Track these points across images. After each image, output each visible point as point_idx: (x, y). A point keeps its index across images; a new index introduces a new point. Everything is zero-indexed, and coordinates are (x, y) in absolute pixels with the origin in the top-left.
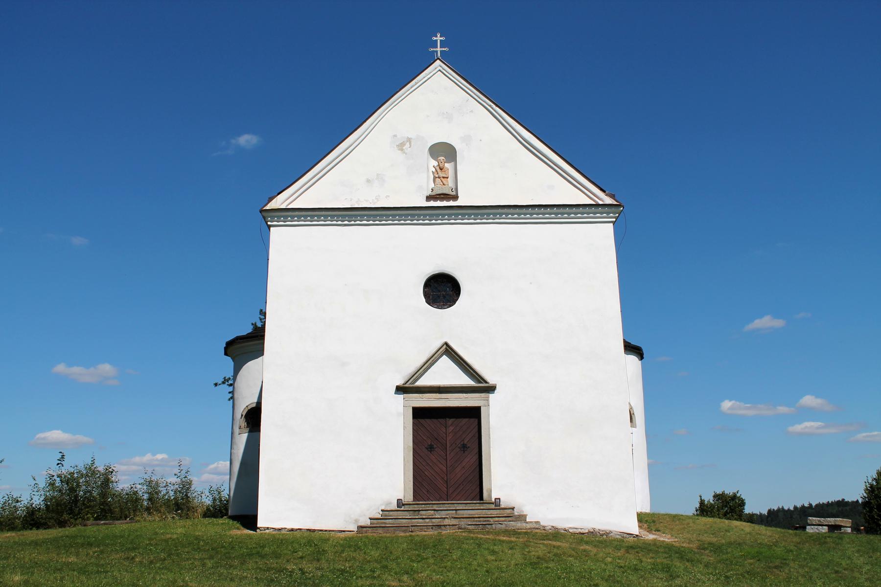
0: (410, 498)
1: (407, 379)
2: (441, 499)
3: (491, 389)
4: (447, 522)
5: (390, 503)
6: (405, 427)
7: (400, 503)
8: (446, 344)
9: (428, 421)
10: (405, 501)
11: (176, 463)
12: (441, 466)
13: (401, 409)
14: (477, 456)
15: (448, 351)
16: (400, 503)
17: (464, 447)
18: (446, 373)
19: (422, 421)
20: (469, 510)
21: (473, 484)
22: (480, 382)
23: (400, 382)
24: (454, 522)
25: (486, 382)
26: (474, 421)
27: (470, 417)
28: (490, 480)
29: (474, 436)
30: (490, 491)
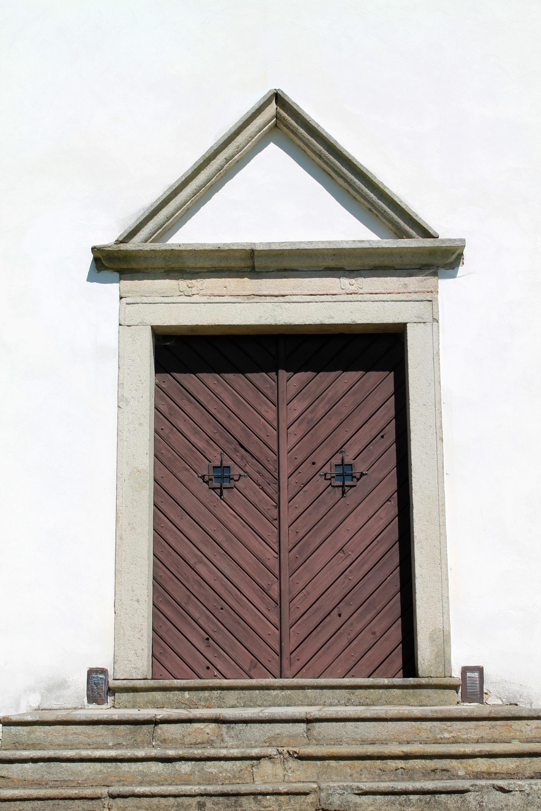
0: (137, 663)
1: (130, 223)
2: (258, 666)
3: (443, 260)
4: (267, 776)
5: (62, 685)
6: (122, 402)
7: (99, 685)
8: (277, 97)
9: (210, 378)
10: (118, 675)
11: (345, 552)
12: (255, 544)
13: (110, 333)
14: (392, 509)
15: (285, 123)
16: (99, 685)
17: (345, 477)
18: (277, 204)
19: (190, 380)
20: (358, 714)
21: (384, 615)
22: (401, 234)
23: (107, 238)
24: (300, 775)
25: (426, 233)
26: (385, 381)
27: (367, 369)
28: (444, 599)
29: (381, 434)
30: (443, 640)
